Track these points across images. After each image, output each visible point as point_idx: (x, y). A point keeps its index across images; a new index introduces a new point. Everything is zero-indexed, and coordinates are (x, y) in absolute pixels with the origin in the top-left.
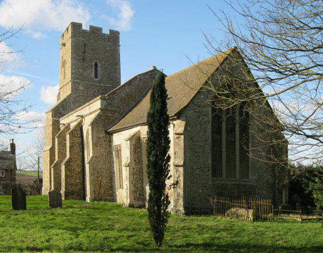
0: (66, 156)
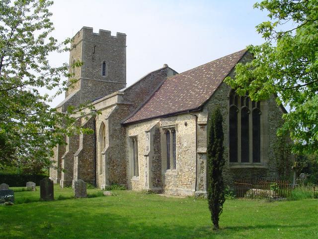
0: (78, 146)
